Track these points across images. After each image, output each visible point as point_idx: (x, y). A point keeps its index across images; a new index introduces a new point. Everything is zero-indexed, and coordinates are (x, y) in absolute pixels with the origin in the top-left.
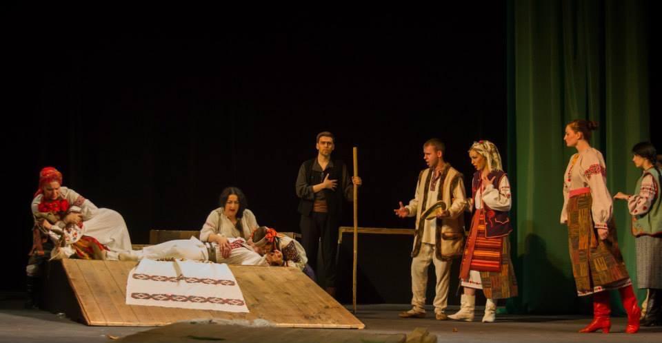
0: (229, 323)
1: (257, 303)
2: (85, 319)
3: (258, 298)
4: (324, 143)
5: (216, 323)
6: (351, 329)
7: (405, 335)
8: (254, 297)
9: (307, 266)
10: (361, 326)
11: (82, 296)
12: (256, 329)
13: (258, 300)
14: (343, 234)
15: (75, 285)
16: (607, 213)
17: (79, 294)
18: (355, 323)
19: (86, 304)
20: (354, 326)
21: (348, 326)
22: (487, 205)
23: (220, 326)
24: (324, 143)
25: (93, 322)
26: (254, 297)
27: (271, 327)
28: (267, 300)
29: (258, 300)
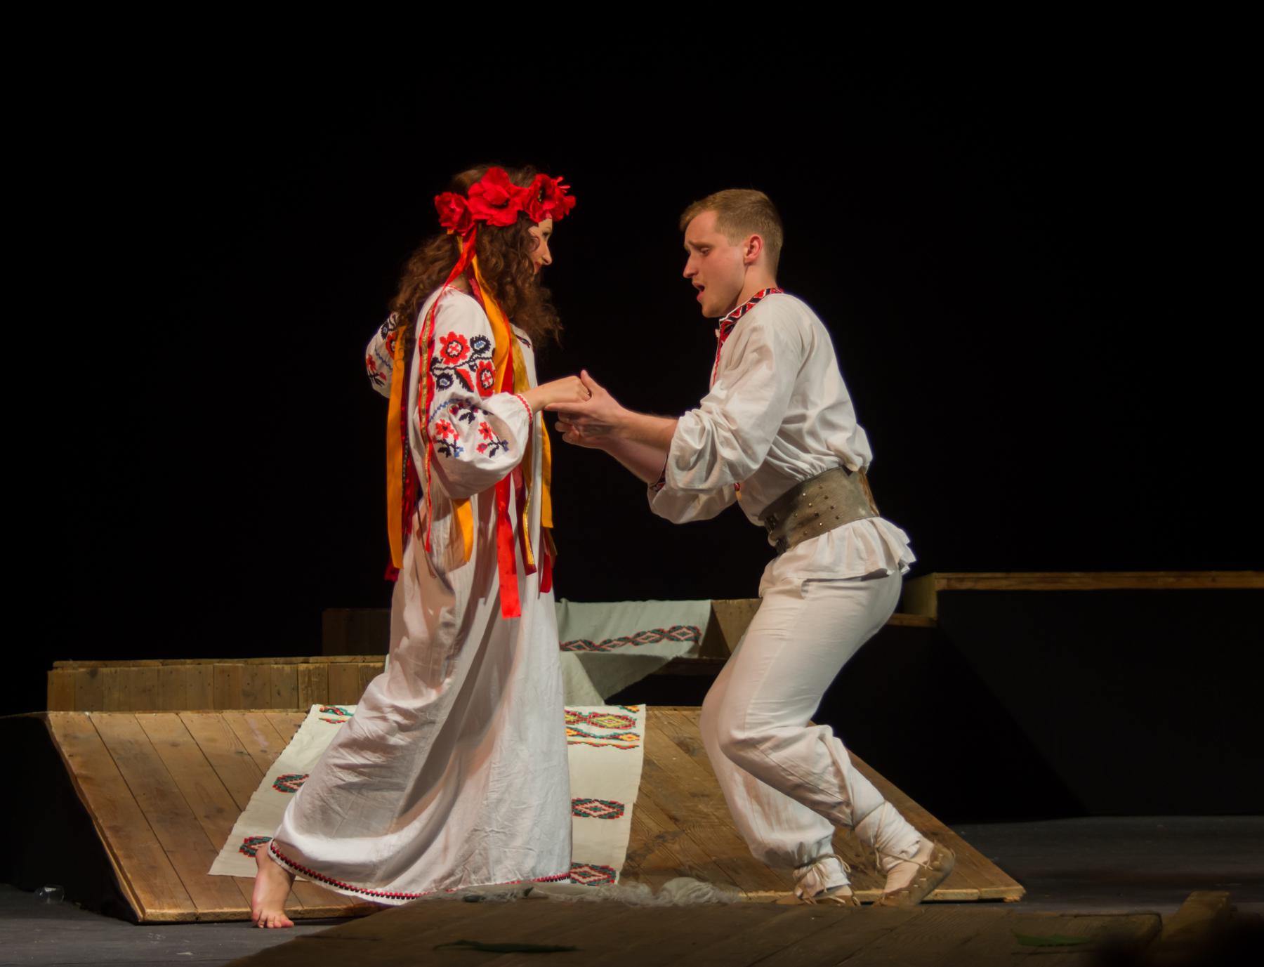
0: (589, 898)
1: (672, 827)
2: (127, 904)
3: (674, 813)
4: (560, 179)
5: (546, 897)
6: (981, 901)
7: (1159, 915)
8: (663, 810)
9: (373, 881)
10: (1014, 892)
11: (116, 830)
12: (674, 911)
13: (674, 819)
14: (942, 595)
15: (90, 797)
16: (543, 434)
17: (103, 823)
18: (992, 884)
19: (129, 857)
20: (988, 892)
21: (972, 893)
22: (619, 688)
23: (561, 906)
24: (560, 179)
25: (152, 912)
26: (663, 810)
27: (722, 904)
28: (706, 816)
29: (674, 819)
